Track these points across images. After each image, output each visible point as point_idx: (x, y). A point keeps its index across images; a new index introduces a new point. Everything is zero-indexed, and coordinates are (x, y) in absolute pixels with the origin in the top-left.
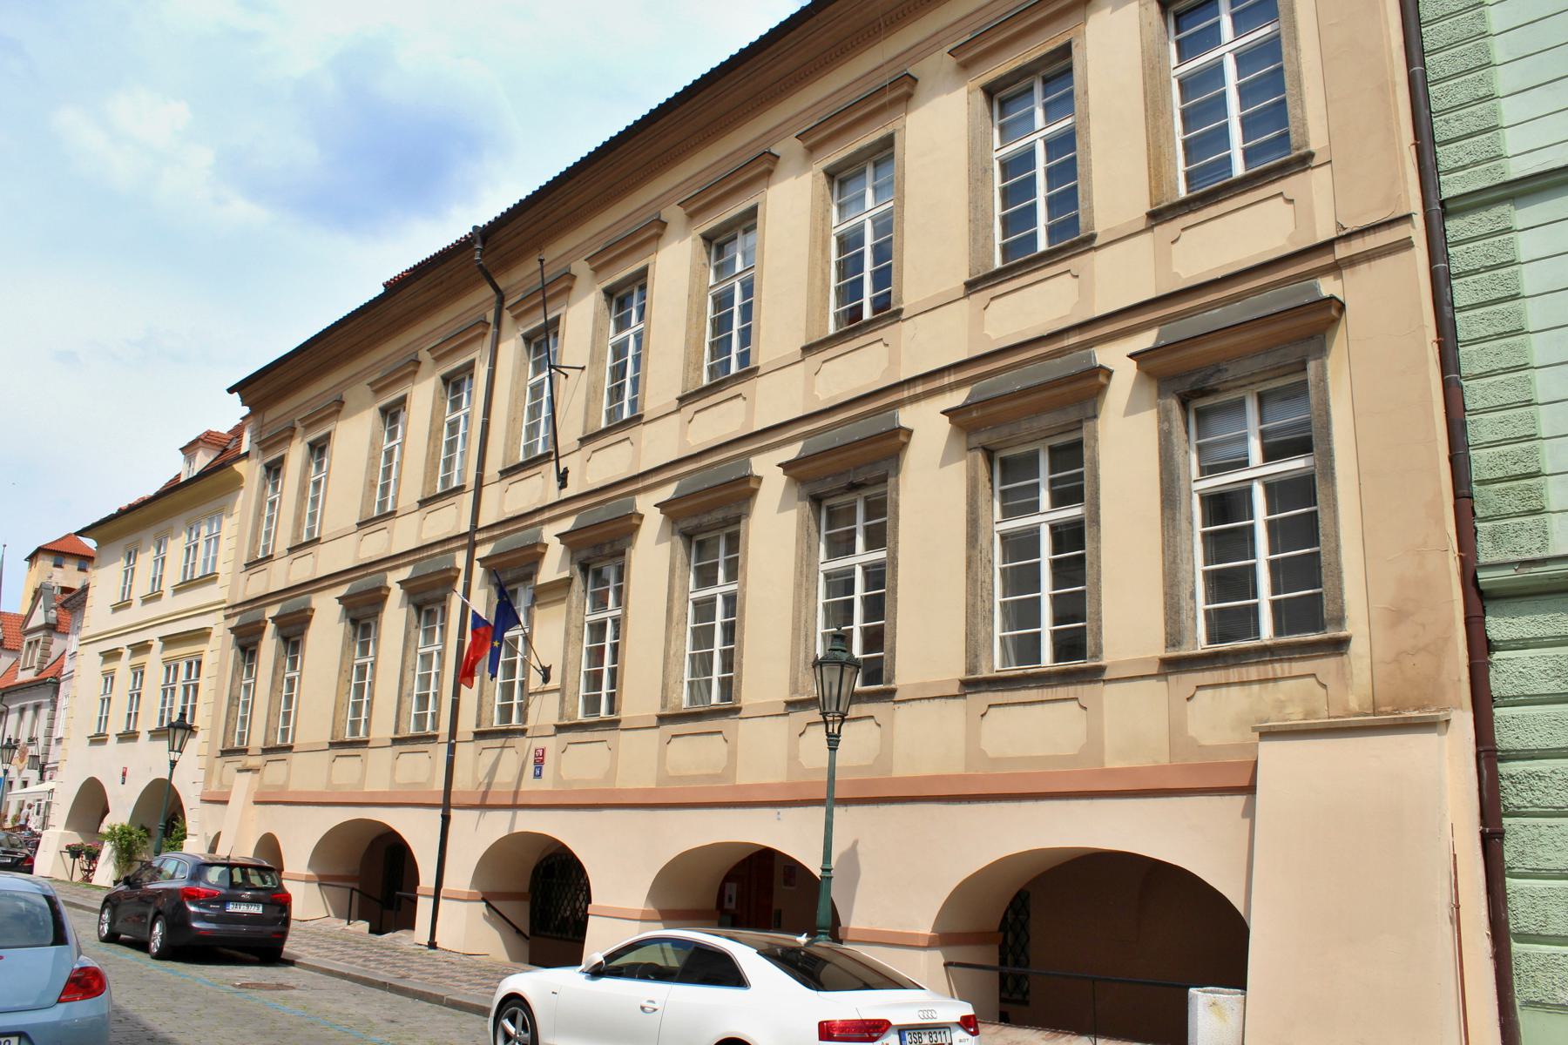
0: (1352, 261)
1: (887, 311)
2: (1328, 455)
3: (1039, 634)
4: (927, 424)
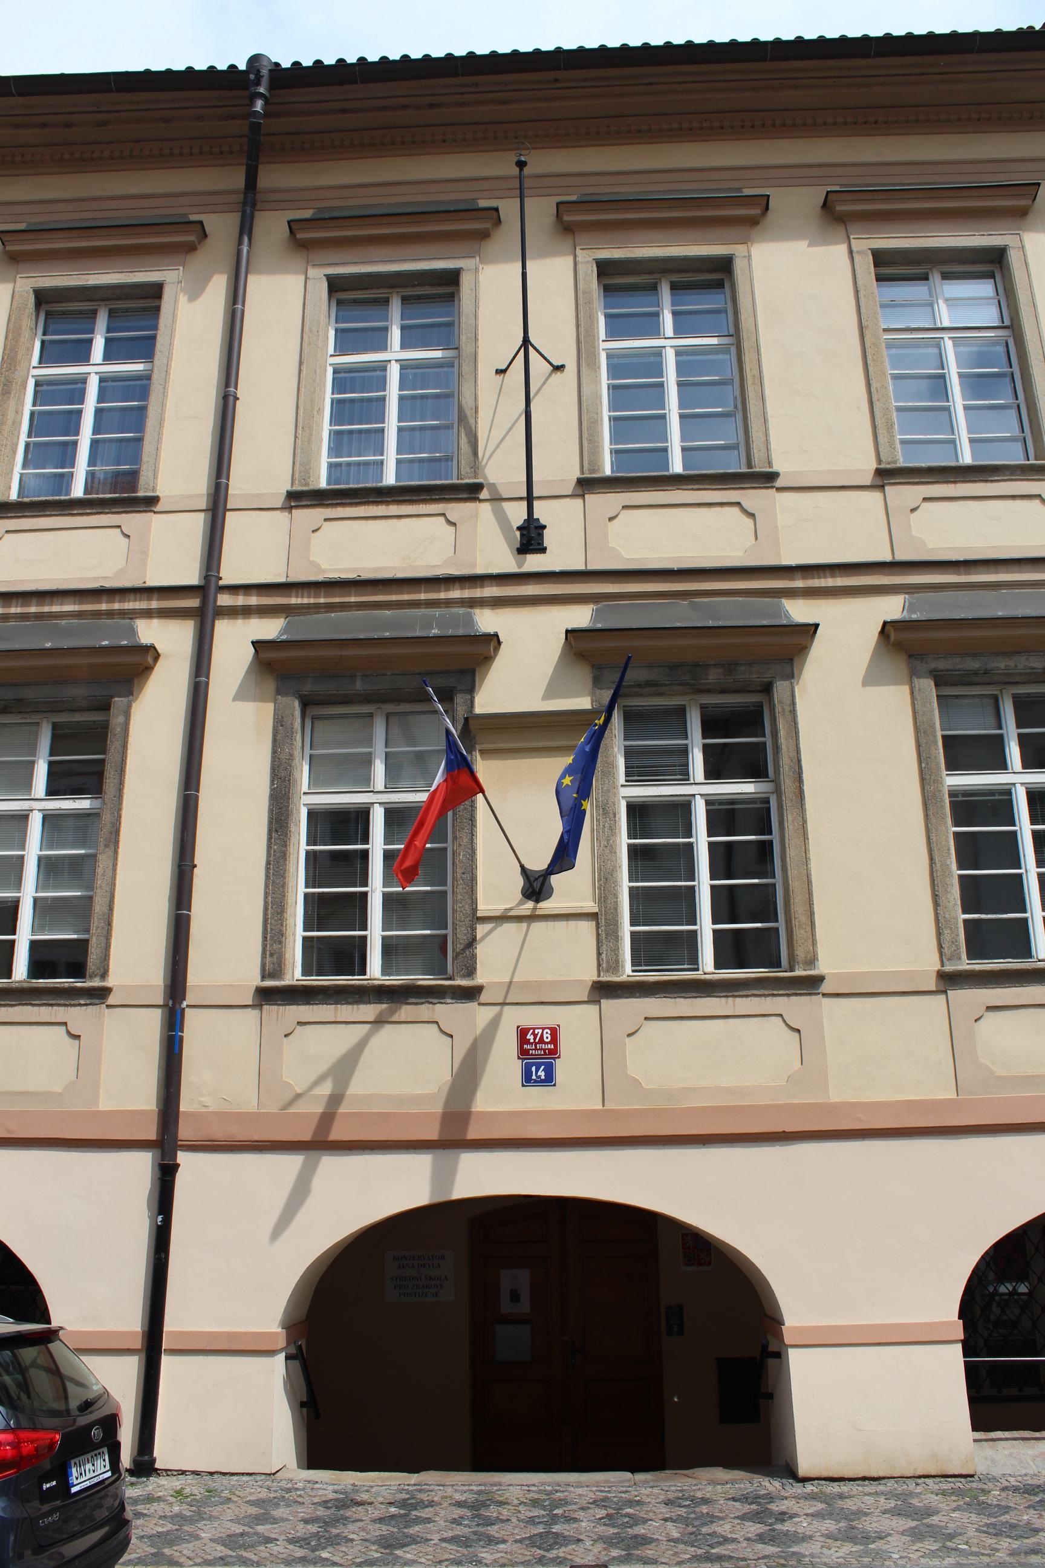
2: (776, 782)
3: (12, 943)
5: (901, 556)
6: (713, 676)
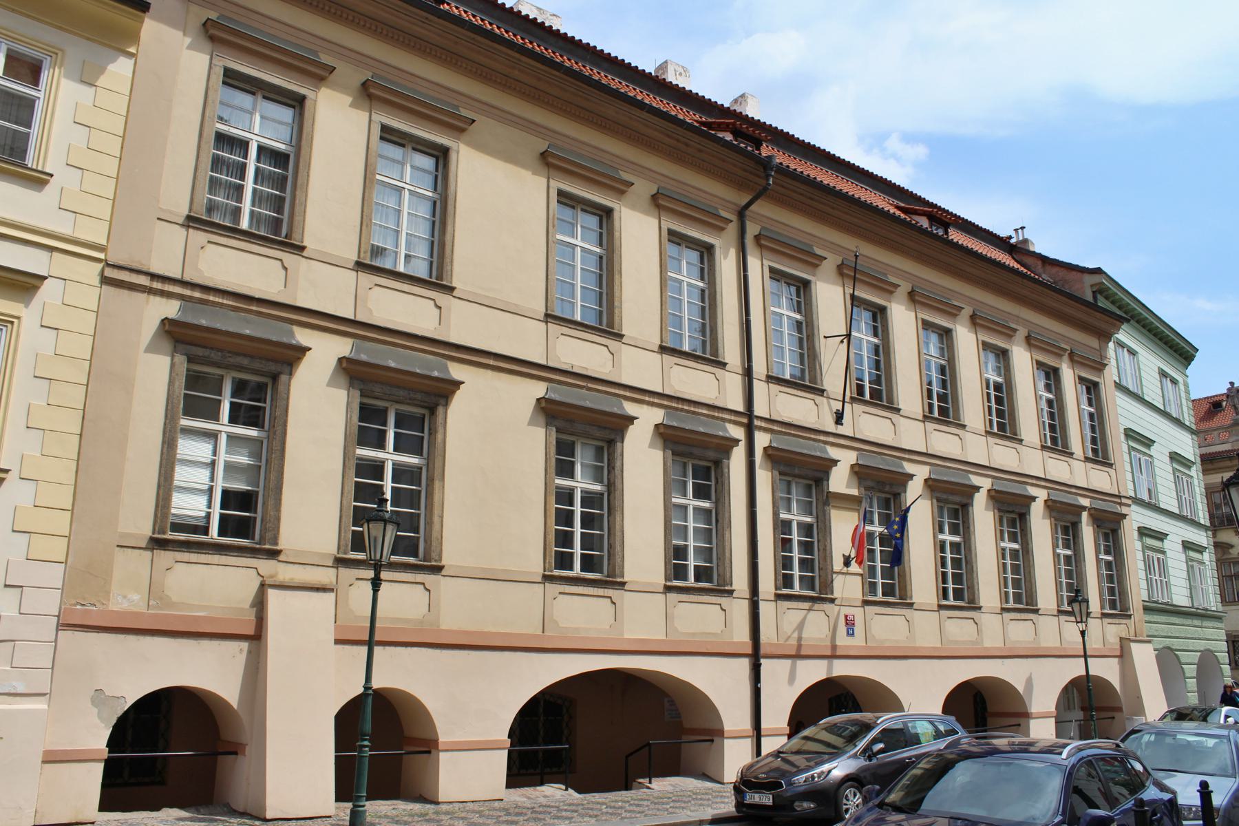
5: (551, 364)
6: (887, 488)
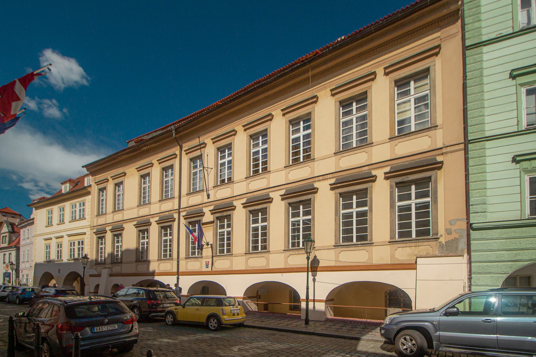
0: (446, 153)
1: (308, 158)
4: (324, 187)
